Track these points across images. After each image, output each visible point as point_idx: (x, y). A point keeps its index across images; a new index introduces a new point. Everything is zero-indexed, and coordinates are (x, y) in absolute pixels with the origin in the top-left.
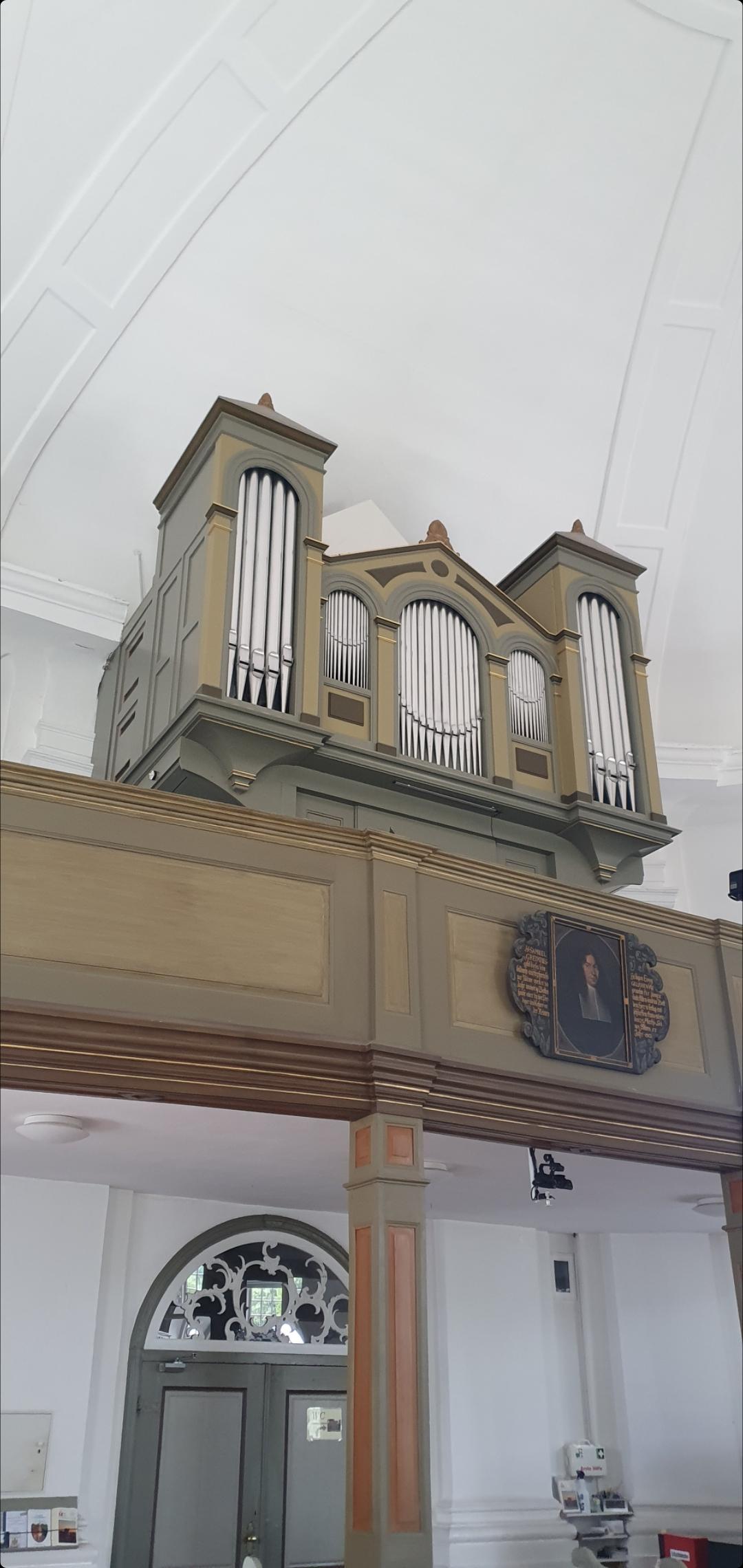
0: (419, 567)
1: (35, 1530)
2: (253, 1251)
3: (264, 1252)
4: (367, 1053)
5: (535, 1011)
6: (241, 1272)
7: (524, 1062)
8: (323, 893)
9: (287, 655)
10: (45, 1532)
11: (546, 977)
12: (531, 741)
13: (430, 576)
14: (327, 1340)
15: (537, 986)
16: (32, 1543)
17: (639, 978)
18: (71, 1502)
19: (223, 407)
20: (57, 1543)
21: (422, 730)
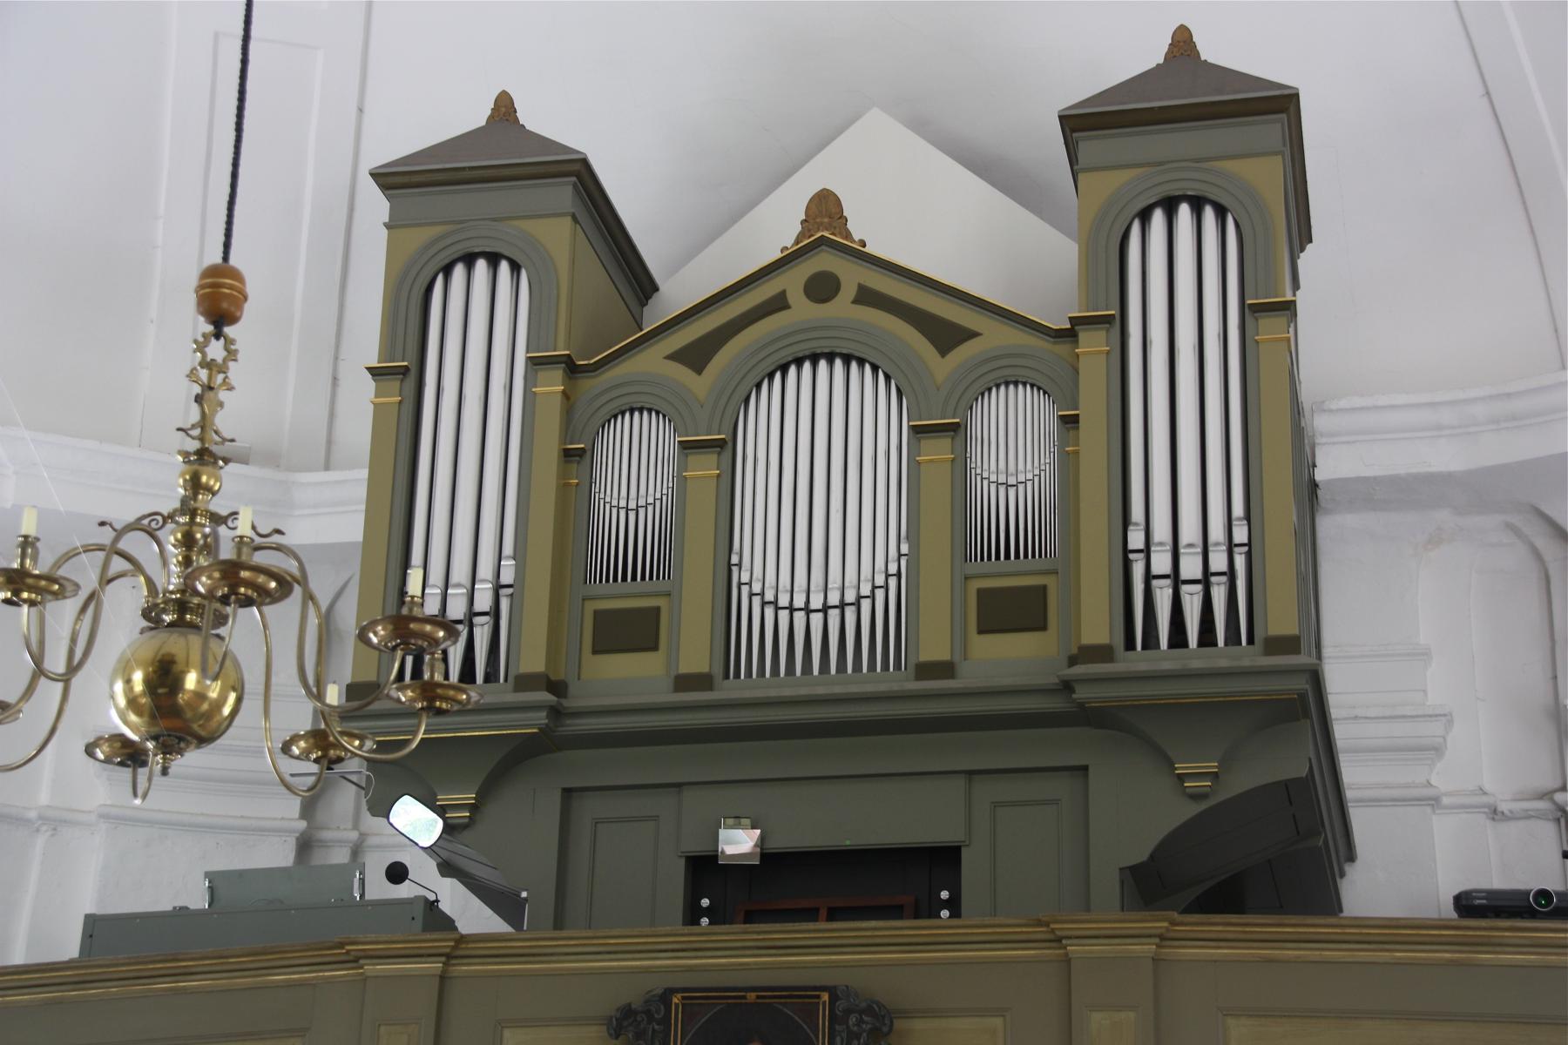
0: (779, 303)
9: (1240, 535)
13: (802, 310)
21: (769, 611)
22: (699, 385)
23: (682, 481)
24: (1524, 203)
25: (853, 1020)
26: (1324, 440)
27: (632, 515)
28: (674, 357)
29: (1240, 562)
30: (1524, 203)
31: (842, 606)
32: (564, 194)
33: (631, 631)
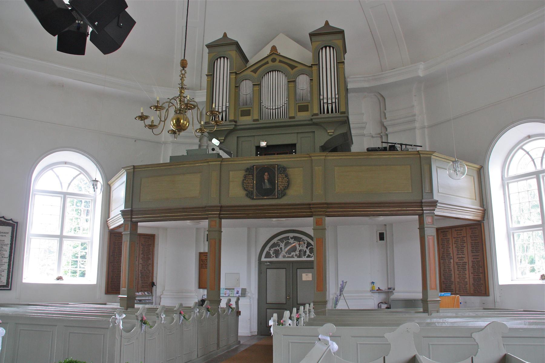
0: (267, 63)
2: (287, 238)
4: (310, 204)
6: (284, 243)
13: (271, 64)
14: (307, 257)
28: (252, 71)
32: (234, 47)
33: (246, 113)
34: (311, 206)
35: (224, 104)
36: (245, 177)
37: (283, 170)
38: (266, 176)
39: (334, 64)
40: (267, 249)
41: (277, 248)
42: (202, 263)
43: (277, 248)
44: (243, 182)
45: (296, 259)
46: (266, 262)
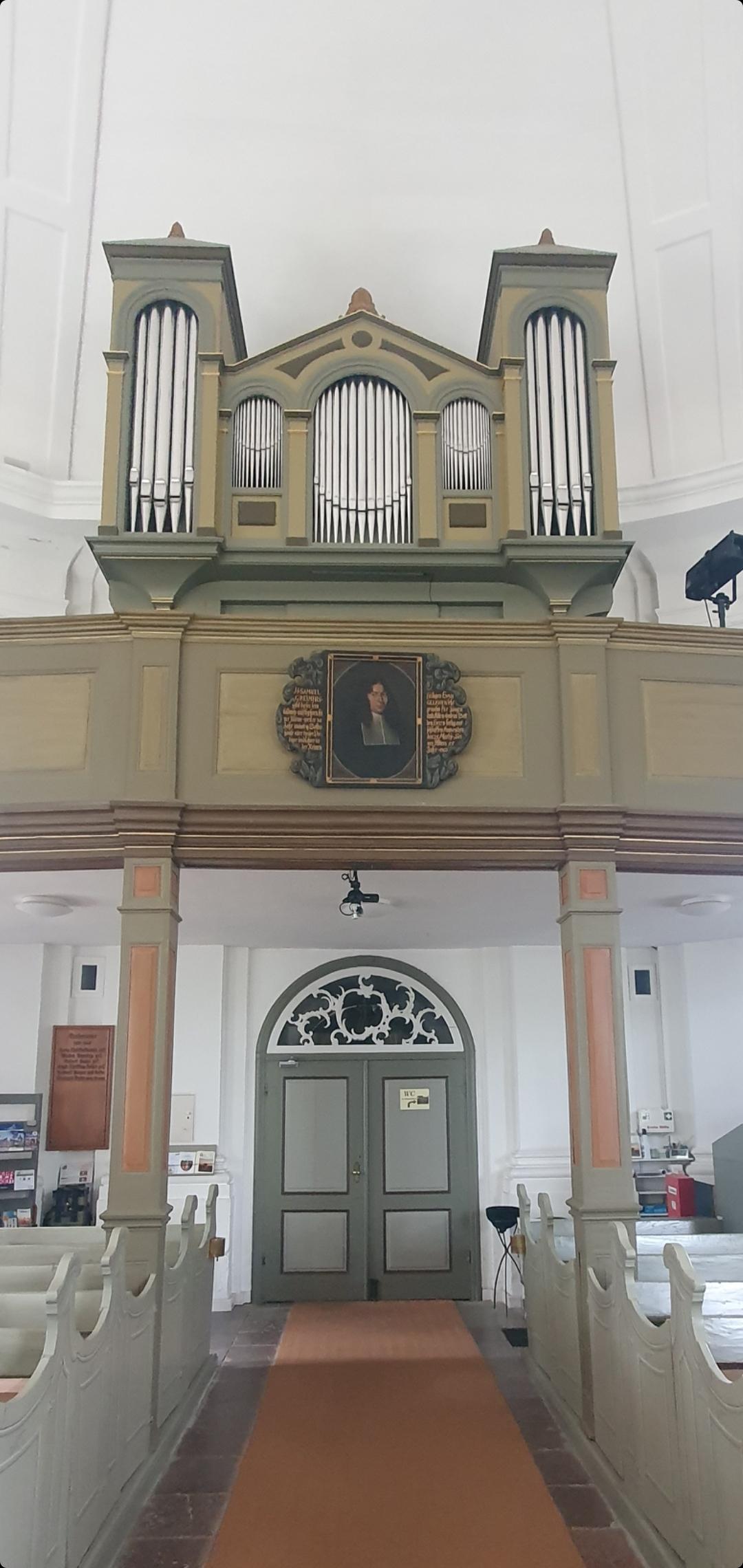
0: (338, 346)
1: (183, 1164)
2: (352, 982)
3: (360, 982)
4: (557, 814)
5: (304, 747)
6: (342, 998)
7: (302, 796)
8: (90, 681)
9: (587, 482)
10: (191, 1165)
11: (320, 713)
12: (472, 492)
13: (351, 350)
14: (415, 1042)
15: (308, 723)
16: (180, 1171)
17: (436, 696)
18: (213, 1148)
19: (502, 260)
20: (197, 1172)
21: (336, 510)
22: (296, 385)
23: (286, 435)
24: (647, 410)
25: (437, 672)
26: (24, 1113)
27: (258, 454)
28: (282, 368)
29: (587, 495)
30: (647, 410)
31: (376, 510)
33: (261, 515)
34: (564, 820)
35: (176, 472)
36: (290, 694)
37: (446, 677)
38: (376, 697)
39: (575, 376)
40: (286, 1015)
41: (321, 1013)
42: (61, 1061)
43: (321, 1013)
44: (281, 719)
45: (380, 1047)
46: (286, 1057)
